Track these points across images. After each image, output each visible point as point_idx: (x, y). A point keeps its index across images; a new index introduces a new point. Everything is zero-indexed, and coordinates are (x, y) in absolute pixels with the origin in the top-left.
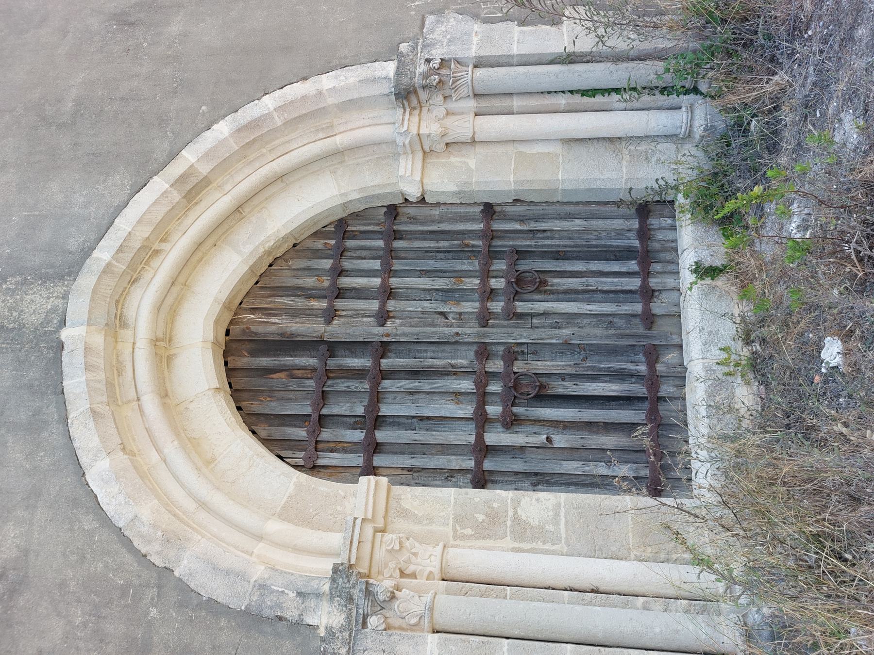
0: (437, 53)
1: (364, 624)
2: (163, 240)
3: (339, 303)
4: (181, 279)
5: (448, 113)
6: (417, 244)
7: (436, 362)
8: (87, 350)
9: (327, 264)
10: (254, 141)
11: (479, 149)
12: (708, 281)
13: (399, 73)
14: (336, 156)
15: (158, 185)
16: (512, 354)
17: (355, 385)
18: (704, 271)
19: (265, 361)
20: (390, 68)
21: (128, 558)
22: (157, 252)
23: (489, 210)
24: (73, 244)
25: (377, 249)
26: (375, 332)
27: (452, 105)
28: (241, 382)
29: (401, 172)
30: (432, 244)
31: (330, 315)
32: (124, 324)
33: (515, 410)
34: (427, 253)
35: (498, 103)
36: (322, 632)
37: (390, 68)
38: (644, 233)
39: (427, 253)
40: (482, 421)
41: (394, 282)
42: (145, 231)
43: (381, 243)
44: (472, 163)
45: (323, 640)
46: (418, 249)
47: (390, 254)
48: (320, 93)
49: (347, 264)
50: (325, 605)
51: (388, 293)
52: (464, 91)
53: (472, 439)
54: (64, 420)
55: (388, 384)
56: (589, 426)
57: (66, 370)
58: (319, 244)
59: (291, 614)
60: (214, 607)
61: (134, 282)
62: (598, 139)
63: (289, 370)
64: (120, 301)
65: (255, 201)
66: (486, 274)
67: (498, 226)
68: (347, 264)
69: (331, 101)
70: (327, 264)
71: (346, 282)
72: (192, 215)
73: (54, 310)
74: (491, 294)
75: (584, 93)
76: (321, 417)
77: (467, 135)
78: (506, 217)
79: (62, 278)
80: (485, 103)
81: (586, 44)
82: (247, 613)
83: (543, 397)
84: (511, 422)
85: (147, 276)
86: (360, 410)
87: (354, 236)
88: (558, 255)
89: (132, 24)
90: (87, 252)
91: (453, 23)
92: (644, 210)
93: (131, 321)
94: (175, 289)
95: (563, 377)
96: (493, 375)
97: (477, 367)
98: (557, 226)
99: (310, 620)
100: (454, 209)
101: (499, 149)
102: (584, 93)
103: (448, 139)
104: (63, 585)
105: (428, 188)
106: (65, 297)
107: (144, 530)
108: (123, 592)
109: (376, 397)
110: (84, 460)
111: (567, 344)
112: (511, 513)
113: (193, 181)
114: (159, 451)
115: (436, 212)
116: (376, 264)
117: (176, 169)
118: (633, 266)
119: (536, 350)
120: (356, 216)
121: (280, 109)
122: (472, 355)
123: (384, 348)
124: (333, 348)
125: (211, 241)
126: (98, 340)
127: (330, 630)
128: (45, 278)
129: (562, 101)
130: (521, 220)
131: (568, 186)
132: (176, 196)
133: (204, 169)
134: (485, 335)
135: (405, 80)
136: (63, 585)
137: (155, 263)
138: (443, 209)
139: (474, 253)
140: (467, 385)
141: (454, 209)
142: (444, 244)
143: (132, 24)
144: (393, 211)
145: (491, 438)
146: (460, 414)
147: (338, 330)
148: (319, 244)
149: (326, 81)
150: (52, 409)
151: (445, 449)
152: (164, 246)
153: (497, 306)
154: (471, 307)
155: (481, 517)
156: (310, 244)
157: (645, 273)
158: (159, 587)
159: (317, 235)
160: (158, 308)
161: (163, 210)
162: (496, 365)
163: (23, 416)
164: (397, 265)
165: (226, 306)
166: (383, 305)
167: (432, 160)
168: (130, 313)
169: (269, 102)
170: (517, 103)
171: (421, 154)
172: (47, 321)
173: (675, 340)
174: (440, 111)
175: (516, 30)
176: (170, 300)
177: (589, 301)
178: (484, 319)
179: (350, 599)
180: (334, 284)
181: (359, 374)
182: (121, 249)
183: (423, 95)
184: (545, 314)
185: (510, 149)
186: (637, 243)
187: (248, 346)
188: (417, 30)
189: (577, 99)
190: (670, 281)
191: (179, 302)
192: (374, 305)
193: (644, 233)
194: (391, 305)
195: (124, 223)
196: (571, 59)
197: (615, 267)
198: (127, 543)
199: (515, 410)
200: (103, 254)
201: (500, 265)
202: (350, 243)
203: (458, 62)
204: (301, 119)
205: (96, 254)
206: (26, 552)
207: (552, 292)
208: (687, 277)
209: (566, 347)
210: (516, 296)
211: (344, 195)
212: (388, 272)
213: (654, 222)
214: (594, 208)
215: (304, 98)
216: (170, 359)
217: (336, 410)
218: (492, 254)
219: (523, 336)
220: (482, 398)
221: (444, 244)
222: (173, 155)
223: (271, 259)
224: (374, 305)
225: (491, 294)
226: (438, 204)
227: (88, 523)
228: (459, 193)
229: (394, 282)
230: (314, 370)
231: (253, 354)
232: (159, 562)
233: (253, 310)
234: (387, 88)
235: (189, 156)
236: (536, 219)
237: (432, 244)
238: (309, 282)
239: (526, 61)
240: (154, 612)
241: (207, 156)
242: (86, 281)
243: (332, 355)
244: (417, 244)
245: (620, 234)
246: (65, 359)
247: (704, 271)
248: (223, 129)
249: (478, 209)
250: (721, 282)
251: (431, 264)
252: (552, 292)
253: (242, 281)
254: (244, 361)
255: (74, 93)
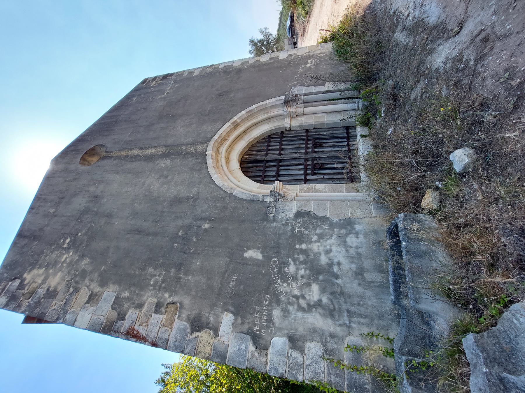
0: (295, 94)
1: (278, 200)
2: (228, 137)
3: (269, 152)
4: (231, 146)
5: (297, 108)
6: (288, 139)
7: (294, 163)
8: (212, 155)
9: (266, 144)
10: (250, 115)
11: (305, 116)
12: (364, 138)
13: (285, 98)
14: (269, 119)
15: (228, 124)
16: (313, 160)
17: (273, 169)
18: (363, 136)
19: (250, 165)
20: (283, 97)
21: (222, 192)
22: (227, 139)
23: (307, 131)
24: (209, 136)
25: (278, 141)
26: (279, 157)
27: (298, 105)
28: (244, 170)
29: (285, 121)
30: (293, 139)
31: (267, 155)
32: (219, 154)
33: (309, 263)
34: (291, 140)
35: (309, 104)
36: (268, 202)
37: (283, 97)
38: (348, 133)
39: (291, 140)
40: (306, 174)
41: (283, 147)
42: (225, 134)
43: (280, 139)
44: (303, 119)
45: (268, 204)
46: (289, 140)
47: (282, 141)
48: (266, 104)
49: (271, 144)
50: (269, 197)
51: (281, 149)
52: (301, 102)
53: (303, 178)
54: (207, 168)
55: (281, 168)
56: (334, 174)
57: (207, 159)
58: (264, 141)
59: (261, 199)
60: (242, 200)
61: (221, 145)
62: (335, 112)
63: (256, 167)
64: (218, 148)
65: (249, 130)
66: (307, 144)
67: (309, 134)
68: (271, 144)
69: (269, 105)
70: (266, 144)
71: (270, 148)
72: (235, 132)
73: (205, 148)
74: (309, 148)
75: (331, 100)
76: (264, 181)
77: (301, 113)
78: (311, 132)
79: (206, 143)
80: (306, 104)
81: (331, 88)
82: (250, 200)
83: (322, 168)
84: (313, 174)
85: (224, 144)
86: (274, 174)
87: (272, 138)
88: (325, 139)
89: (222, 95)
90: (212, 137)
91: (298, 87)
92: (347, 128)
93: (220, 153)
94: (230, 148)
95: (327, 164)
96: (309, 165)
97: (305, 163)
98: (325, 133)
99: (265, 200)
100: (298, 131)
101: (310, 116)
102: (331, 100)
103: (297, 114)
104: (207, 198)
105: (291, 125)
106: (207, 146)
107: (226, 187)
108: (221, 198)
109: (278, 171)
110: (211, 175)
111: (328, 157)
112: (314, 188)
113: (236, 123)
114: (227, 177)
115: (294, 132)
116: (278, 144)
117: (232, 121)
118: (345, 140)
119: (320, 158)
120: (273, 134)
121: (257, 107)
122: (303, 161)
123: (280, 161)
124: (268, 161)
125: (238, 139)
126: (214, 154)
127: (270, 202)
128: (202, 143)
129: (326, 102)
130: (316, 132)
131: (327, 122)
132: (232, 127)
133: (239, 121)
134: (306, 156)
135: (287, 99)
136: (207, 198)
137: (226, 142)
138: (295, 131)
139: (303, 140)
140: (302, 167)
141: (298, 131)
142: (296, 138)
143: (222, 95)
144: (282, 133)
145: (308, 177)
146: (300, 173)
147: (269, 158)
148: (264, 141)
149: (268, 101)
150: (204, 166)
151: (299, 165)
152: (228, 138)
153: (310, 150)
154: (303, 151)
155: (306, 189)
156: (262, 141)
157: (348, 141)
158: (229, 197)
159: (263, 139)
160: (227, 151)
161: (229, 129)
162: (310, 162)
163: (198, 168)
164: (283, 143)
165: (241, 153)
166: (280, 152)
167: (293, 119)
168: (220, 151)
169: (254, 106)
170: (314, 104)
171: (290, 118)
172: (203, 150)
173: (359, 177)
174: (295, 107)
175: (314, 87)
176: (228, 151)
177: (334, 148)
178: (306, 153)
179: (275, 196)
180: (267, 148)
181: (274, 166)
182: (219, 137)
183: (291, 103)
184: (322, 151)
185: (313, 115)
186: (346, 135)
187: (246, 162)
188: (290, 90)
189: (330, 102)
190: (355, 143)
191: (231, 151)
192: (278, 152)
193: (348, 133)
194: (282, 152)
195: (220, 132)
196: (327, 92)
197: (341, 140)
198: (222, 189)
199: (309, 263)
200: (216, 137)
201: (310, 142)
202: (271, 140)
203: (299, 95)
204: (261, 110)
205: (214, 138)
206: (199, 193)
207: (324, 147)
208: (359, 138)
209: (328, 157)
210: (315, 148)
211: (271, 128)
212: (281, 145)
213: (350, 131)
214: (335, 129)
215: (262, 105)
216: (228, 163)
217: (268, 174)
218: (308, 140)
219: (317, 156)
220: (306, 169)
221: (296, 138)
222: (232, 118)
223: (252, 144)
224: (278, 152)
225: (309, 148)
226: (294, 130)
227: (213, 186)
228: (299, 126)
229: (283, 147)
230: (263, 166)
231: (247, 164)
232: (229, 192)
233: (247, 155)
234: (282, 102)
235: (235, 118)
236: (320, 132)
237: (293, 139)
238: (261, 148)
239: (316, 93)
240: (228, 201)
241: (239, 118)
242: (212, 143)
243: (267, 163)
244: (288, 139)
245: (341, 133)
246: (207, 157)
247: (363, 136)
248: (243, 112)
249: (304, 131)
250: (367, 138)
251: (292, 143)
252: (324, 147)
253: (245, 148)
254: (245, 165)
255: (209, 109)
